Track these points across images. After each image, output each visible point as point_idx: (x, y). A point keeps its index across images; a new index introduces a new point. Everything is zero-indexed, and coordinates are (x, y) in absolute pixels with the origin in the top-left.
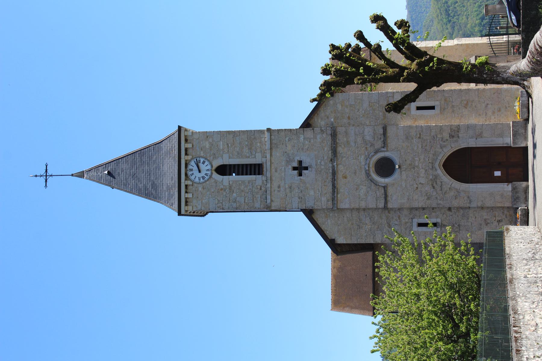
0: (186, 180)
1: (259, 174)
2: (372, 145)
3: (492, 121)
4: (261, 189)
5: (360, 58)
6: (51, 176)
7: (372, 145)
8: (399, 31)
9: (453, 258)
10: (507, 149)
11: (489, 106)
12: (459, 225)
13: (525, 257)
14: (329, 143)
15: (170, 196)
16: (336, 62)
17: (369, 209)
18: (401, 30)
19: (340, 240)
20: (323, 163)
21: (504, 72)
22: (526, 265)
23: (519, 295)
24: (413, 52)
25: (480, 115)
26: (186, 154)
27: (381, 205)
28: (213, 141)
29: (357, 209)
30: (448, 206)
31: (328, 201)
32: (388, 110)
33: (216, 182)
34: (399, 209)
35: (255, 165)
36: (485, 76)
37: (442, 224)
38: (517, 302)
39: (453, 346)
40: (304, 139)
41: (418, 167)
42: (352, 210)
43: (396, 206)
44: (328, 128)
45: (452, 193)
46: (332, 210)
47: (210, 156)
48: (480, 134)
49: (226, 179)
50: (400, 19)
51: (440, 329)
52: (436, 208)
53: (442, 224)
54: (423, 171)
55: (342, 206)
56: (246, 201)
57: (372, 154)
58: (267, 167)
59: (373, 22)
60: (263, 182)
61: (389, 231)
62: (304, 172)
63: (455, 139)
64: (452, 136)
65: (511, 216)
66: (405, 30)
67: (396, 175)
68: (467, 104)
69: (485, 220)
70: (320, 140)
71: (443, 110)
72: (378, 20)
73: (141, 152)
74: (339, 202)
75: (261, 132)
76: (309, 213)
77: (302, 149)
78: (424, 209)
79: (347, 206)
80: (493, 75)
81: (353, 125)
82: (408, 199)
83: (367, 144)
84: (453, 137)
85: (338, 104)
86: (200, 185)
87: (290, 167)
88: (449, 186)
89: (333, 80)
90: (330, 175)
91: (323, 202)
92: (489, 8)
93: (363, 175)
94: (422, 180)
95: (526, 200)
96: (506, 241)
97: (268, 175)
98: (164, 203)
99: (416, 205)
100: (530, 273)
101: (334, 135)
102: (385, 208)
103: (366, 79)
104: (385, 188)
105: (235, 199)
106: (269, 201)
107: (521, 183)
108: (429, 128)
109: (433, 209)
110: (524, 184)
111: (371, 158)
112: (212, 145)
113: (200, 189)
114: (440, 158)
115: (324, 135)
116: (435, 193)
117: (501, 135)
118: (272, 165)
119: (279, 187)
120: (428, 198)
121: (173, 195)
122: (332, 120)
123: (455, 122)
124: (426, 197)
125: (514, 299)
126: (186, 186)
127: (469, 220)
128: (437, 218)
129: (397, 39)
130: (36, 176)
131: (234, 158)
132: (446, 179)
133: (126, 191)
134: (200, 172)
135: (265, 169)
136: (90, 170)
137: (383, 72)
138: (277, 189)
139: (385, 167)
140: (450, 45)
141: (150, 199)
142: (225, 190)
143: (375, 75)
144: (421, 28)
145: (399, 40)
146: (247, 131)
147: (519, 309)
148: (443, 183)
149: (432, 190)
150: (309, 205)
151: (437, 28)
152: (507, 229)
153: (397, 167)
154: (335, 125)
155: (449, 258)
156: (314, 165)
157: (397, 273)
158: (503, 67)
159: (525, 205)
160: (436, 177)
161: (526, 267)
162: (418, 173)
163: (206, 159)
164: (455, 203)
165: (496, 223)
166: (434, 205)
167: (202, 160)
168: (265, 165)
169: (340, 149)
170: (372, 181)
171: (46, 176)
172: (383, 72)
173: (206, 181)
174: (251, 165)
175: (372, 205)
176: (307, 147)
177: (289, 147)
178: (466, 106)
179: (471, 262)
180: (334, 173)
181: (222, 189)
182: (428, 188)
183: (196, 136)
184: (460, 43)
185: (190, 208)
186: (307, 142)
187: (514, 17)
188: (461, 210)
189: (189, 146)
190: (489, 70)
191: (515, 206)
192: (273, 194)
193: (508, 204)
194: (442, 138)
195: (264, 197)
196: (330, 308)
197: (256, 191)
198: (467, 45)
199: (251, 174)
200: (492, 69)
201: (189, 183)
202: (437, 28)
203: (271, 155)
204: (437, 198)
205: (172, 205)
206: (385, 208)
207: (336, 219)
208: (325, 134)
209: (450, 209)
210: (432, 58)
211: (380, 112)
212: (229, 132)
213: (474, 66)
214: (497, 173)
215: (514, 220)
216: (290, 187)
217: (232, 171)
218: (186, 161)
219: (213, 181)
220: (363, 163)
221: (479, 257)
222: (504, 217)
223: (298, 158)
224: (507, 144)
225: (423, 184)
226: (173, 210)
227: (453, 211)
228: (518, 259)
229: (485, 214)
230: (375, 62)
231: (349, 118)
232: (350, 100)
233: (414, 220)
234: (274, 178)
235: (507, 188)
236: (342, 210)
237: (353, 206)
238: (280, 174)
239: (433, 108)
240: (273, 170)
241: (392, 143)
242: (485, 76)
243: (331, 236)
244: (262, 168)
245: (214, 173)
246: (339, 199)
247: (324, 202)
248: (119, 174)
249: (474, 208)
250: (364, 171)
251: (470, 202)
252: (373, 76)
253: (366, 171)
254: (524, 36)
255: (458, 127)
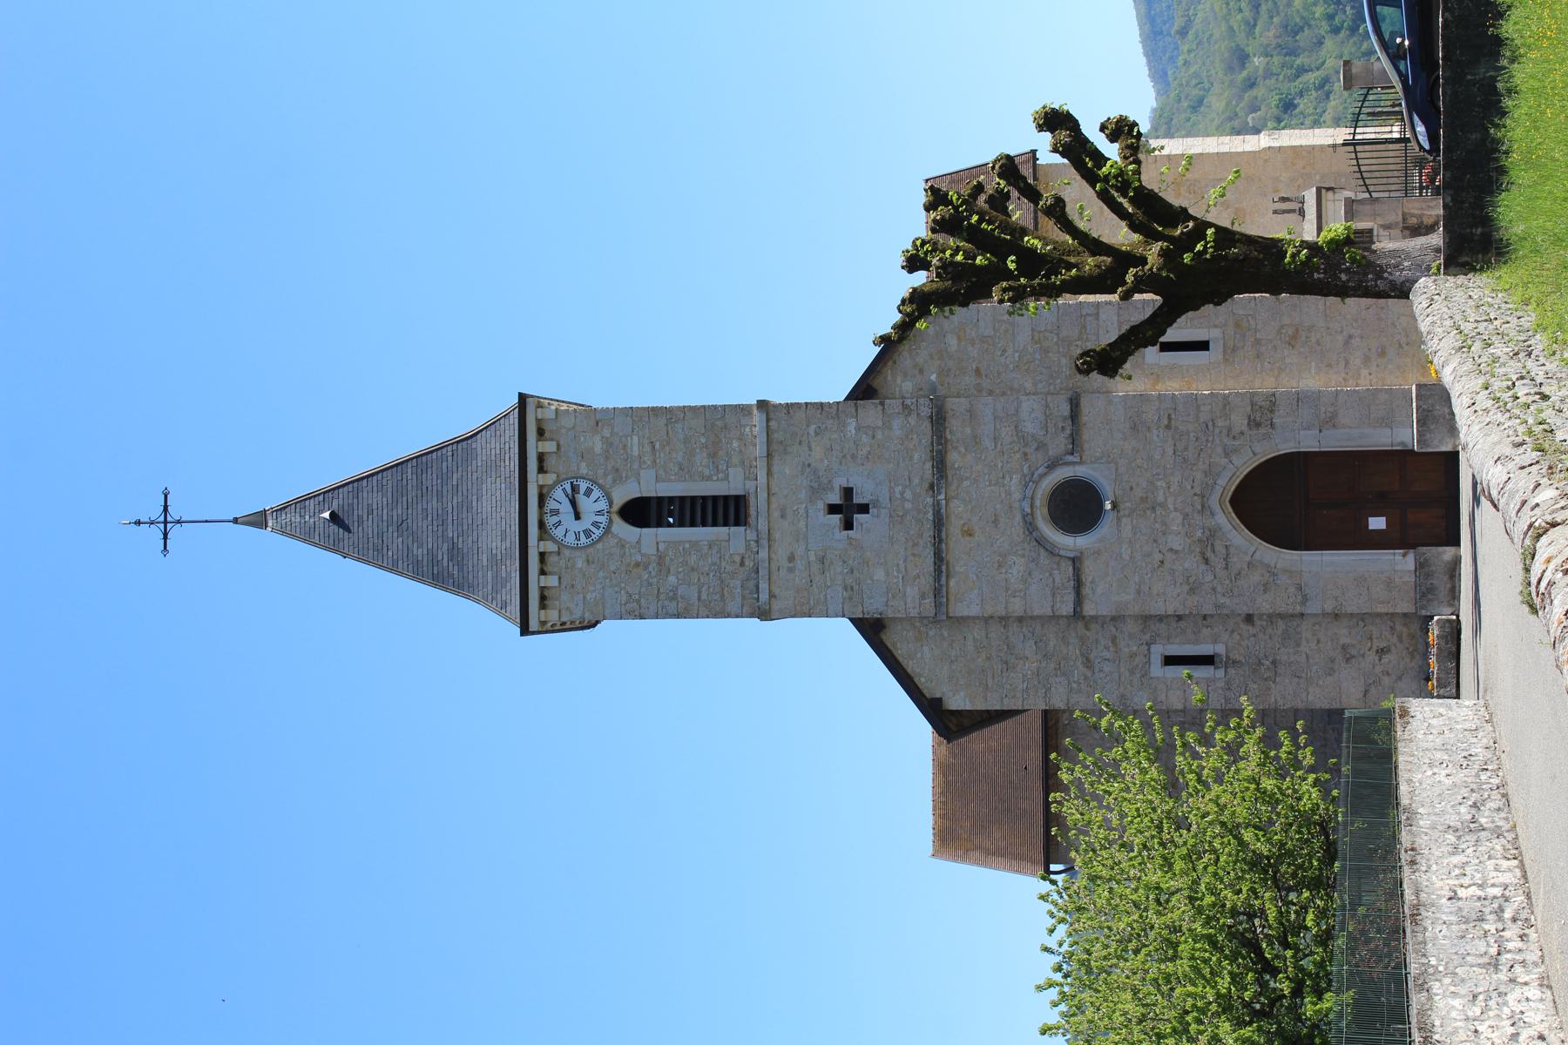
0: (541, 539)
1: (737, 524)
2: (1041, 446)
3: (1361, 382)
4: (742, 564)
5: (1007, 227)
6: (179, 522)
7: (1041, 446)
8: (1112, 151)
9: (1258, 789)
10: (1403, 457)
11: (1355, 342)
12: (1274, 662)
13: (1453, 820)
14: (926, 441)
15: (500, 583)
16: (941, 238)
17: (1032, 618)
18: (1116, 145)
19: (957, 701)
20: (908, 495)
21: (1396, 266)
22: (1456, 850)
23: (1437, 971)
24: (1151, 212)
25: (1329, 366)
26: (541, 470)
27: (1066, 608)
28: (612, 433)
29: (1002, 618)
30: (1245, 610)
31: (923, 597)
32: (1084, 371)
33: (622, 544)
34: (1114, 619)
35: (726, 498)
36: (1343, 277)
37: (1228, 657)
38: (1430, 998)
39: (1259, 1029)
40: (858, 429)
41: (1163, 505)
42: (987, 620)
43: (1105, 610)
44: (922, 401)
45: (1256, 577)
46: (935, 620)
47: (605, 475)
48: (1331, 418)
49: (650, 537)
50: (1114, 114)
51: (1224, 983)
52: (1212, 616)
53: (1228, 657)
54: (1179, 517)
55: (960, 609)
56: (704, 597)
57: (1041, 470)
58: (758, 505)
59: (1040, 128)
60: (748, 547)
61: (1086, 678)
62: (859, 518)
63: (1262, 431)
64: (1254, 424)
65: (1412, 637)
66: (1128, 147)
67: (1105, 528)
68: (1295, 336)
69: (1344, 647)
70: (899, 432)
71: (1230, 352)
72: (1055, 120)
73: (420, 461)
74: (952, 598)
75: (743, 410)
76: (872, 630)
77: (854, 457)
78: (1180, 618)
79: (974, 611)
80: (1366, 275)
81: (990, 393)
82: (1139, 592)
83: (1026, 445)
84: (1258, 425)
85: (949, 336)
86: (578, 553)
87: (821, 505)
88: (1248, 558)
89: (935, 286)
90: (929, 526)
91: (909, 600)
92: (1354, 71)
93: (1016, 528)
94: (1176, 542)
95: (1454, 594)
96: (1401, 759)
97: (763, 525)
98: (485, 601)
99: (1158, 608)
100: (1466, 881)
101: (938, 419)
102: (1077, 615)
103: (1025, 286)
104: (1076, 562)
105: (674, 590)
106: (764, 597)
107: (1441, 549)
108: (1195, 400)
109: (1205, 617)
110: (1448, 553)
111: (1037, 483)
112: (611, 444)
113: (580, 564)
114: (1222, 482)
115: (912, 420)
116: (1209, 577)
117: (1387, 422)
118: (773, 499)
119: (791, 558)
120: (1192, 591)
121: (508, 579)
122: (933, 377)
123: (1264, 384)
124: (1186, 588)
125: (1423, 987)
126: (542, 555)
127: (1302, 648)
128: (1215, 642)
129: (1106, 179)
130: (138, 523)
131: (670, 481)
132: (1241, 539)
133: (381, 567)
134: (578, 517)
135: (752, 511)
136: (283, 509)
137: (1069, 266)
138: (785, 563)
139: (1077, 506)
140: (1248, 148)
141: (446, 589)
142: (646, 568)
143: (1047, 277)
144: (1169, 7)
145: (1113, 182)
146: (704, 407)
147: (1437, 1023)
148: (1232, 550)
149: (1203, 567)
150: (873, 606)
151: (1212, 9)
152: (1405, 713)
153: (1108, 506)
154: (942, 391)
155: (1247, 789)
156: (884, 499)
157: (1114, 796)
158: (1394, 253)
159: (1450, 610)
160: (1213, 533)
161: (1456, 859)
162: (1164, 524)
163: (594, 482)
164: (1264, 604)
165: (1372, 657)
166: (1208, 609)
167: (583, 486)
168: (752, 501)
169: (953, 457)
170: (1041, 542)
171: (166, 522)
172: (1069, 266)
173: (594, 543)
174: (715, 498)
175: (1041, 608)
176: (864, 452)
177: (818, 452)
178: (1292, 342)
179: (1310, 794)
180: (939, 522)
181: (637, 565)
182: (1191, 563)
183: (567, 422)
184: (1276, 144)
185: (552, 616)
186: (865, 439)
187: (1420, 129)
188: (1280, 622)
189: (548, 447)
190: (1353, 260)
191: (1424, 613)
192: (774, 577)
193: (1405, 607)
194: (1230, 429)
195: (751, 584)
196: (931, 851)
197: (729, 568)
198: (1296, 150)
199: (715, 524)
200: (1364, 257)
201: (549, 546)
202: (1212, 9)
203: (769, 473)
204: (1214, 589)
205: (504, 605)
206: (1077, 615)
207: (945, 644)
208: (914, 416)
209: (1249, 619)
210: (1202, 225)
211: (1065, 365)
212: (655, 411)
213: (1313, 248)
214: (1377, 523)
215: (1421, 647)
216: (822, 560)
217: (665, 512)
218: (541, 487)
219: (612, 541)
220: (1017, 496)
221: (1327, 776)
222: (1395, 640)
223: (840, 482)
224: (1402, 443)
225: (1177, 552)
226: (509, 619)
227: (1258, 623)
228: (1434, 828)
229: (1343, 633)
230: (1045, 238)
231: (978, 372)
232: (982, 323)
233: (1153, 648)
234: (777, 535)
235: (1401, 562)
236: (962, 620)
237: (989, 611)
238: (794, 522)
239: (1203, 346)
240: (776, 514)
241: (1093, 440)
242: (1343, 277)
243: (931, 689)
244: (746, 507)
245: (617, 519)
246: (952, 591)
247: (912, 599)
248: (360, 521)
249: (1316, 615)
250: (1018, 517)
251: (1305, 599)
252: (1041, 275)
253: (1024, 517)
254: (1449, 199)
255: (1272, 402)
